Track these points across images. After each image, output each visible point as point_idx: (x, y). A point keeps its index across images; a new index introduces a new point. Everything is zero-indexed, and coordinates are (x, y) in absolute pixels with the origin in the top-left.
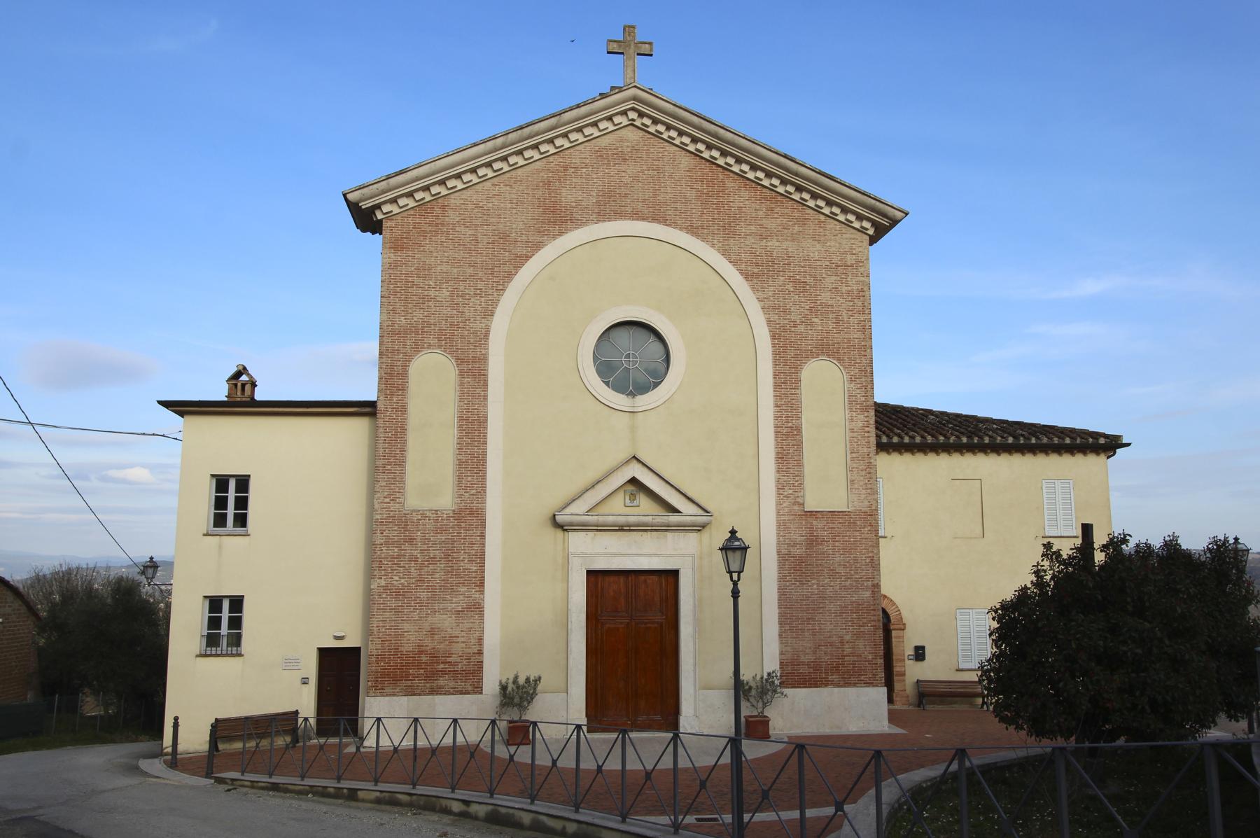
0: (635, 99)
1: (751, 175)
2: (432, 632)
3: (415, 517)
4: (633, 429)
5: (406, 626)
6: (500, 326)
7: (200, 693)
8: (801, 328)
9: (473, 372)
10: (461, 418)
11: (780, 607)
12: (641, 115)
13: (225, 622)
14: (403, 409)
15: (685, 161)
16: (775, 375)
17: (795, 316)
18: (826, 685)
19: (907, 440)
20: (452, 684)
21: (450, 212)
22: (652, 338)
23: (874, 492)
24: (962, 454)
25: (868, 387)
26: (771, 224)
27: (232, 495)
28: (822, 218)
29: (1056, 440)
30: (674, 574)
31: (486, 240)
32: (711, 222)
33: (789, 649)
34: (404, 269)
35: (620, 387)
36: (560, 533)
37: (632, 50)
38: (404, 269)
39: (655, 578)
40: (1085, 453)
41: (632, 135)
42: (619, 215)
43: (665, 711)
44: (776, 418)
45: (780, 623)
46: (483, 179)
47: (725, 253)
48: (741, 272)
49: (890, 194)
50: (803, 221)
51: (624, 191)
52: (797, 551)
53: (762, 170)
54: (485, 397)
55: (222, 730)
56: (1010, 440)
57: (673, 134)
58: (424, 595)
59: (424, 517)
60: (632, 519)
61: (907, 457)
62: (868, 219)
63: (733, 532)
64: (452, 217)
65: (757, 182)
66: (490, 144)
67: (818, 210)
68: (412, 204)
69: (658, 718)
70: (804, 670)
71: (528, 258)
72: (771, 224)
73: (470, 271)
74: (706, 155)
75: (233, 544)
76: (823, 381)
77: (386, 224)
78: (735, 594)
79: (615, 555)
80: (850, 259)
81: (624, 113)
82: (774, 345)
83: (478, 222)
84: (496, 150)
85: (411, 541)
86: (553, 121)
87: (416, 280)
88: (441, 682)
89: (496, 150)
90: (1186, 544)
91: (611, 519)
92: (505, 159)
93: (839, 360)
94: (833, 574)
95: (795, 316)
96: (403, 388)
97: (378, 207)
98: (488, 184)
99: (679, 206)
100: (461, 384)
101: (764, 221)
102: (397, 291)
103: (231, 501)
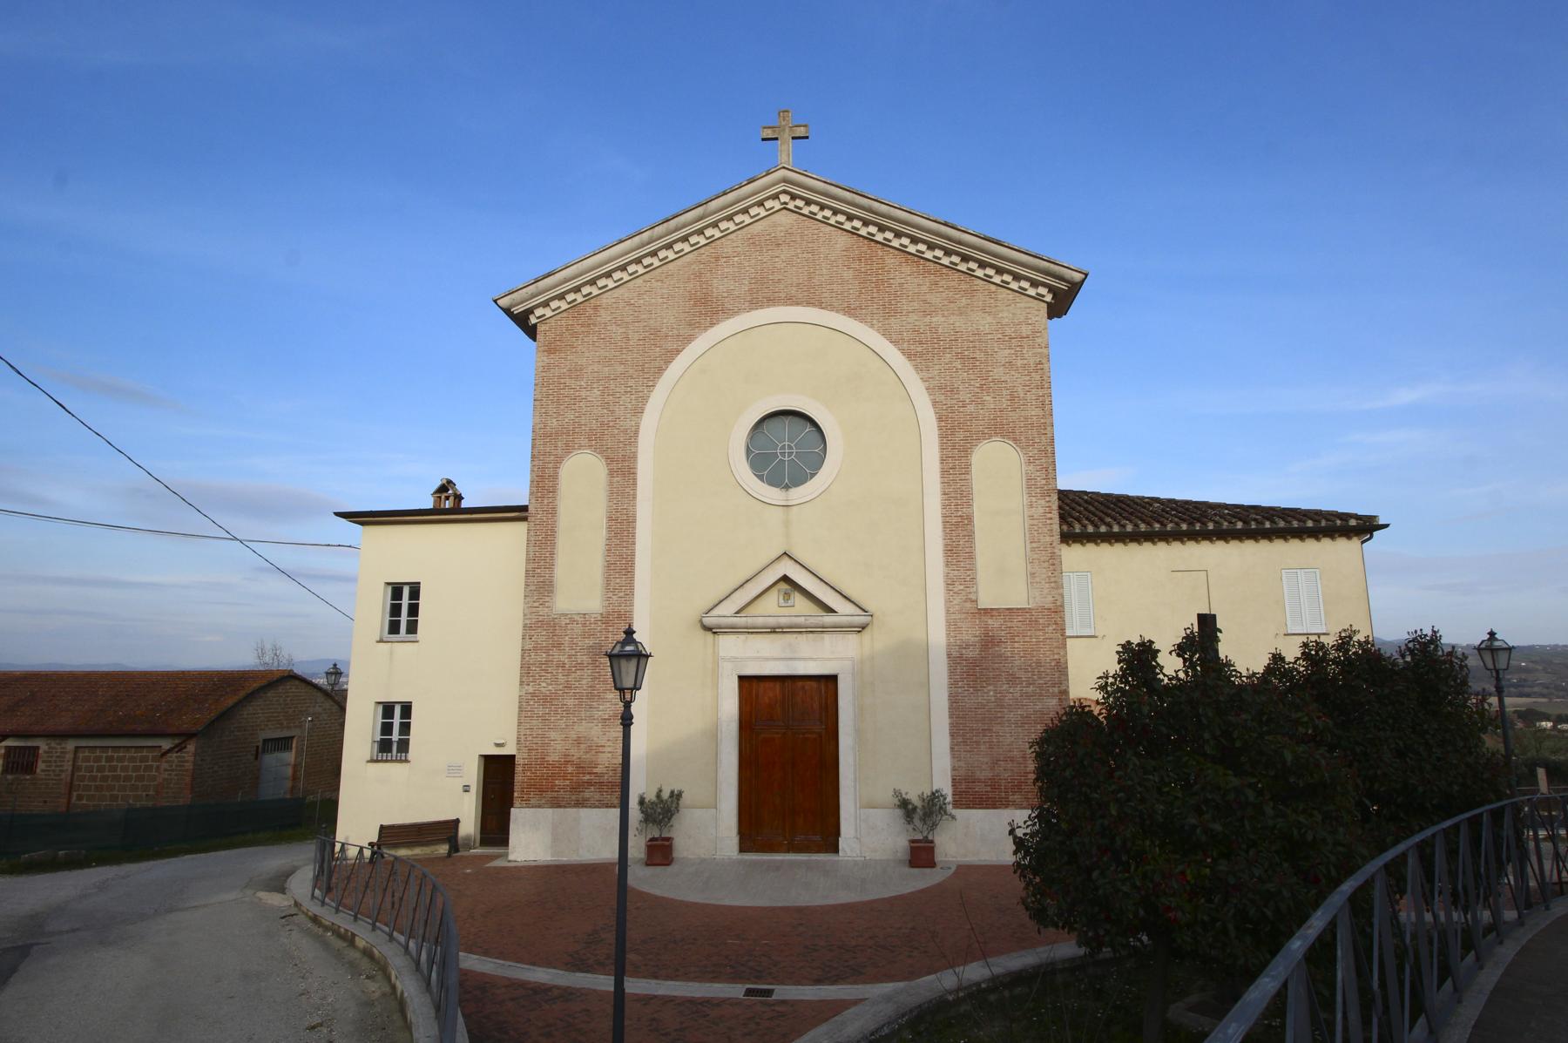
0: (785, 180)
1: (912, 249)
2: (578, 741)
3: (564, 621)
4: (787, 524)
5: (553, 735)
6: (649, 423)
7: (370, 801)
8: (971, 408)
9: (622, 470)
10: (610, 519)
11: (951, 717)
12: (794, 197)
13: (395, 725)
14: (553, 512)
15: (843, 240)
16: (942, 461)
17: (964, 396)
18: (1007, 806)
19: (1116, 529)
20: (597, 796)
21: (602, 312)
22: (809, 428)
23: (1058, 585)
24: (1183, 542)
25: (1050, 470)
26: (935, 299)
27: (405, 602)
28: (993, 288)
29: (1295, 524)
30: (833, 679)
31: (636, 336)
32: (870, 301)
33: (962, 764)
34: (557, 372)
35: (775, 480)
36: (709, 635)
37: (787, 135)
38: (557, 372)
39: (814, 684)
40: (1332, 538)
41: (785, 219)
42: (772, 301)
43: (821, 828)
44: (944, 507)
45: (952, 735)
46: (635, 276)
47: (886, 333)
48: (903, 352)
49: (1070, 258)
50: (971, 293)
51: (777, 277)
52: (971, 653)
53: (924, 242)
54: (634, 497)
55: (390, 835)
56: (1240, 525)
57: (828, 213)
58: (570, 702)
59: (573, 621)
60: (783, 621)
61: (1119, 548)
62: (1044, 285)
63: (1492, 634)
64: (604, 316)
65: (919, 256)
66: (637, 239)
67: (987, 279)
68: (564, 306)
69: (818, 838)
70: (979, 788)
71: (678, 352)
72: (935, 299)
73: (620, 369)
74: (863, 232)
75: (402, 650)
76: (998, 467)
77: (540, 328)
78: (627, 720)
79: (767, 659)
80: (1025, 330)
81: (776, 197)
82: (940, 428)
83: (629, 319)
84: (643, 245)
85: (559, 646)
86: (699, 211)
87: (568, 381)
88: (587, 795)
89: (643, 245)
90: (1448, 638)
91: (760, 621)
92: (654, 254)
93: (1015, 440)
94: (1013, 679)
95: (964, 396)
96: (553, 490)
97: (531, 311)
98: (639, 281)
99: (835, 287)
100: (611, 484)
101: (928, 297)
102: (551, 393)
103: (403, 607)
